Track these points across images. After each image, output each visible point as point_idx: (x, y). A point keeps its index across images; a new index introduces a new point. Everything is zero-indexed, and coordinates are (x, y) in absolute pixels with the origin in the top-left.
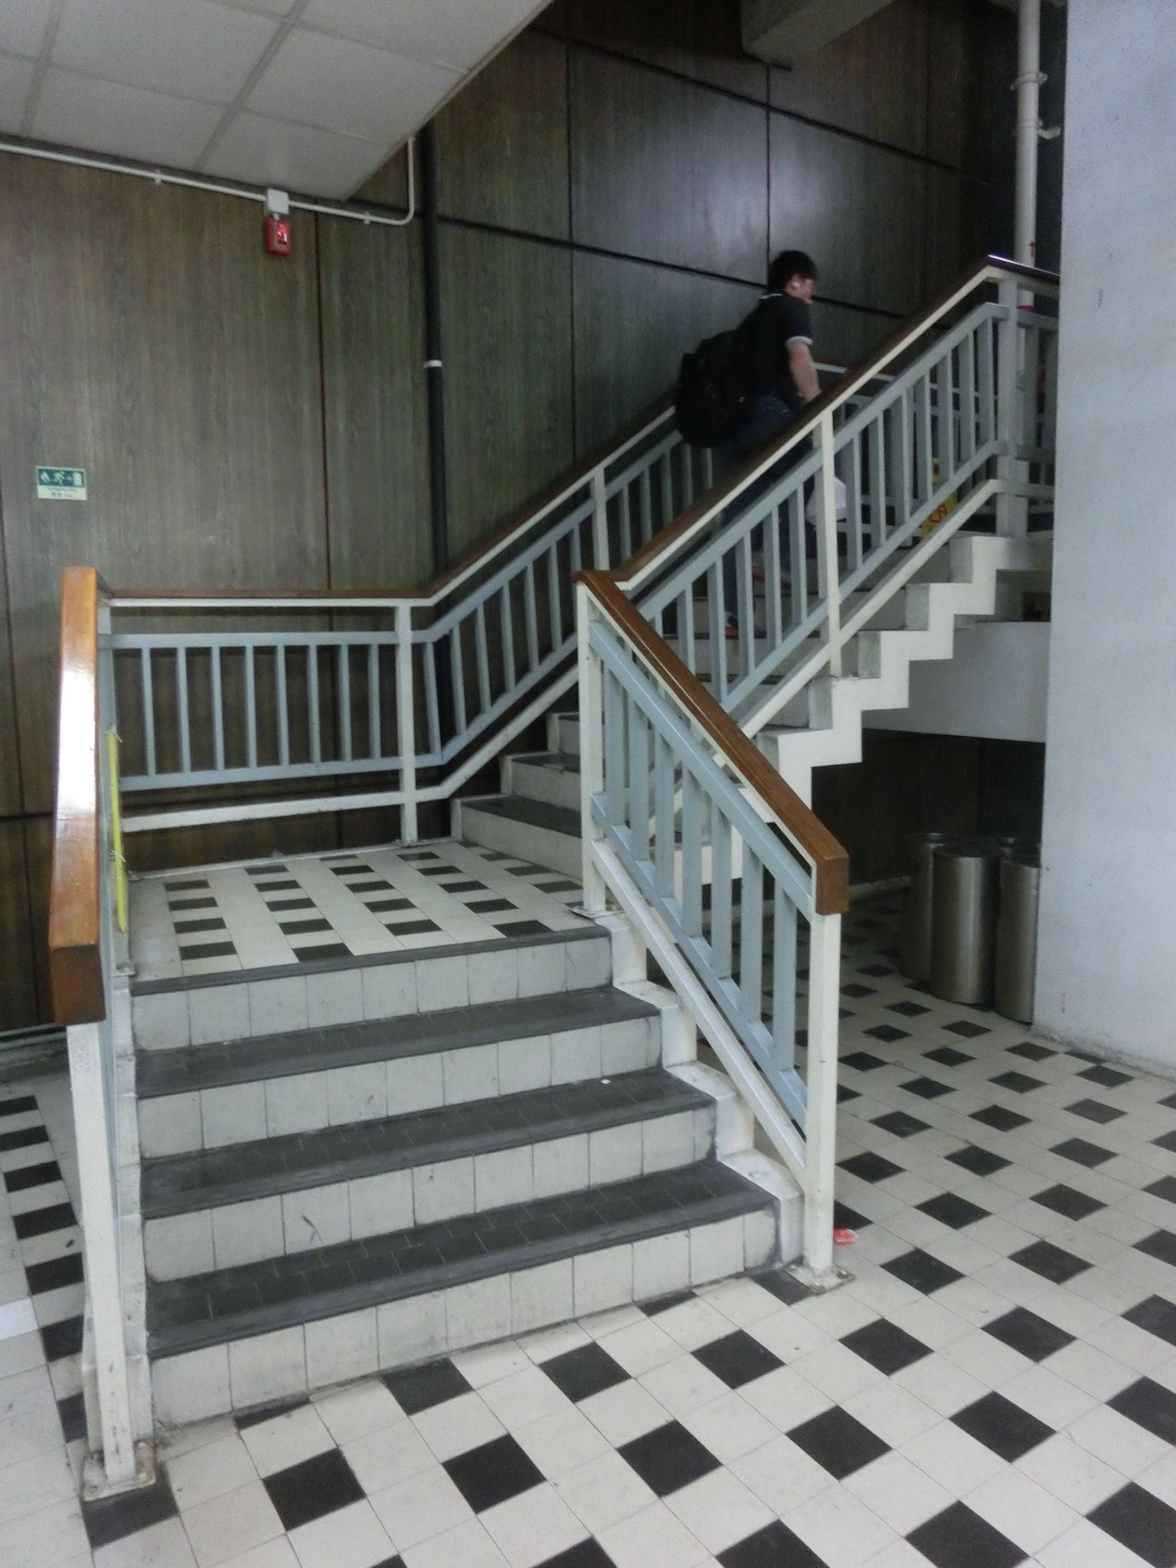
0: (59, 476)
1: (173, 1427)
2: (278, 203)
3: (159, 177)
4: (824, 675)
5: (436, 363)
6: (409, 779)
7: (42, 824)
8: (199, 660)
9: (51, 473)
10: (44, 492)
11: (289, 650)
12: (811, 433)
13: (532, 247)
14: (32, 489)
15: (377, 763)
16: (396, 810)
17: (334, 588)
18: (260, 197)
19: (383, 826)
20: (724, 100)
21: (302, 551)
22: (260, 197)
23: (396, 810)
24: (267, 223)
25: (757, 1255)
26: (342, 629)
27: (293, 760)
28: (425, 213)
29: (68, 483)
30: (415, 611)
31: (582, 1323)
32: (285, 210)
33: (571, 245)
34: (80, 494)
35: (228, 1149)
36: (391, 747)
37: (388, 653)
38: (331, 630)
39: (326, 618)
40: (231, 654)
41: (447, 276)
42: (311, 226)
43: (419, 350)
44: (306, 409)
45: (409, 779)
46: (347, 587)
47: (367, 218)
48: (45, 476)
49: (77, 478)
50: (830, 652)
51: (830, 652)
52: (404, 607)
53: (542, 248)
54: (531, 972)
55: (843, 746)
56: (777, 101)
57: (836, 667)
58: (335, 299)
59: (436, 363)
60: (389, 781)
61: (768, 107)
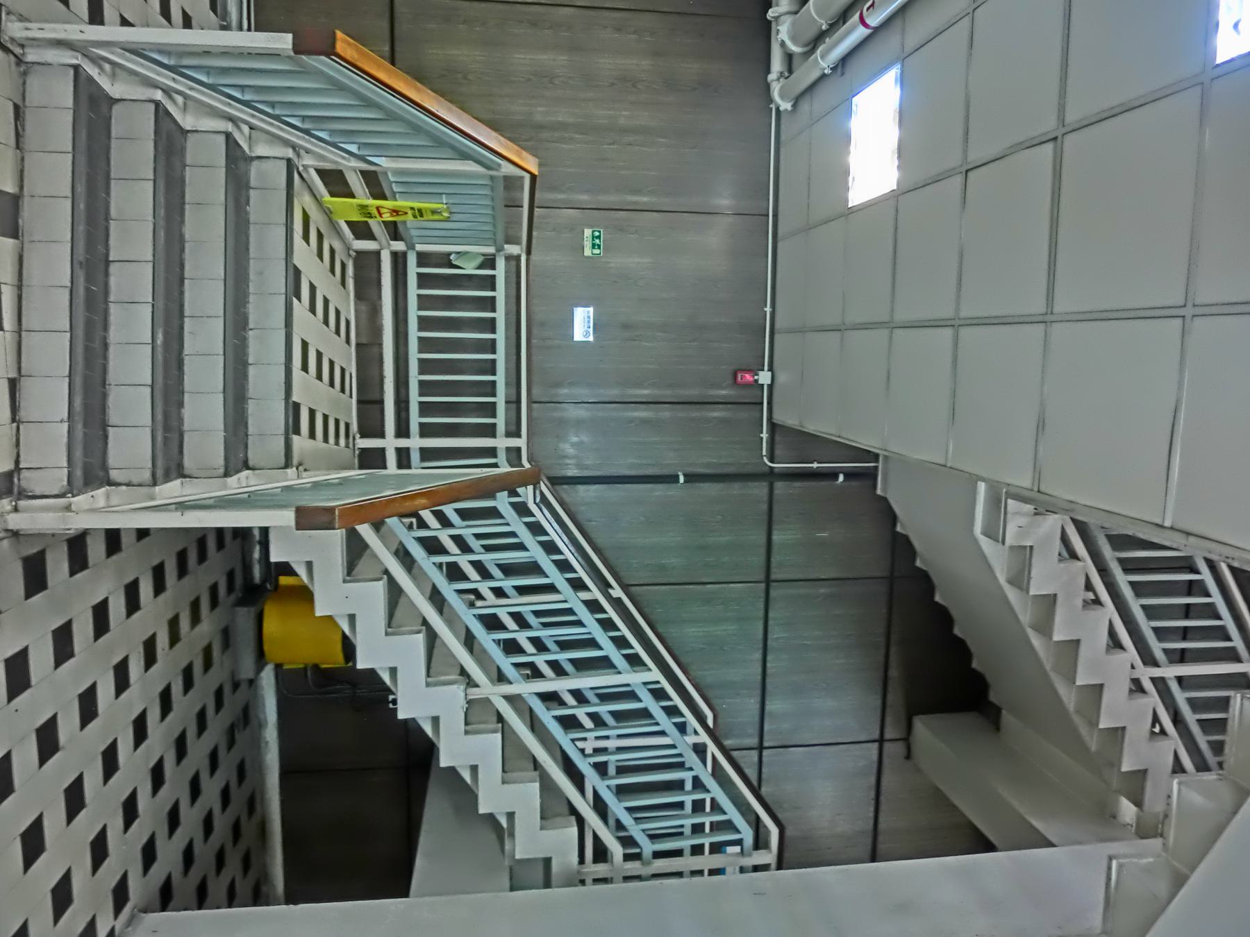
0: (597, 241)
1: (25, 74)
2: (764, 378)
3: (768, 309)
4: (471, 683)
5: (682, 479)
6: (403, 443)
7: (375, 350)
8: (489, 390)
9: (599, 237)
10: (588, 232)
11: (494, 383)
12: (644, 664)
13: (763, 551)
14: (590, 226)
15: (415, 420)
16: (382, 435)
17: (535, 406)
18: (766, 368)
19: (371, 427)
20: (879, 703)
21: (558, 385)
22: (766, 368)
23: (382, 435)
24: (754, 372)
25: (29, 480)
26: (507, 410)
27: (421, 361)
28: (771, 476)
29: (593, 246)
30: (519, 450)
31: (16, 335)
32: (761, 373)
33: (768, 581)
34: (588, 252)
35: (183, 180)
36: (426, 431)
37: (490, 431)
38: (507, 402)
39: (514, 398)
40: (491, 346)
41: (736, 489)
42: (752, 400)
43: (690, 470)
44: (646, 392)
45: (403, 443)
46: (535, 414)
47: (765, 435)
48: (597, 234)
49: (597, 251)
50: (487, 689)
51: (487, 689)
52: (521, 442)
53: (763, 558)
54: (266, 416)
55: (413, 703)
56: (887, 746)
57: (475, 693)
58: (717, 413)
59: (682, 479)
60: (402, 430)
61: (881, 741)
